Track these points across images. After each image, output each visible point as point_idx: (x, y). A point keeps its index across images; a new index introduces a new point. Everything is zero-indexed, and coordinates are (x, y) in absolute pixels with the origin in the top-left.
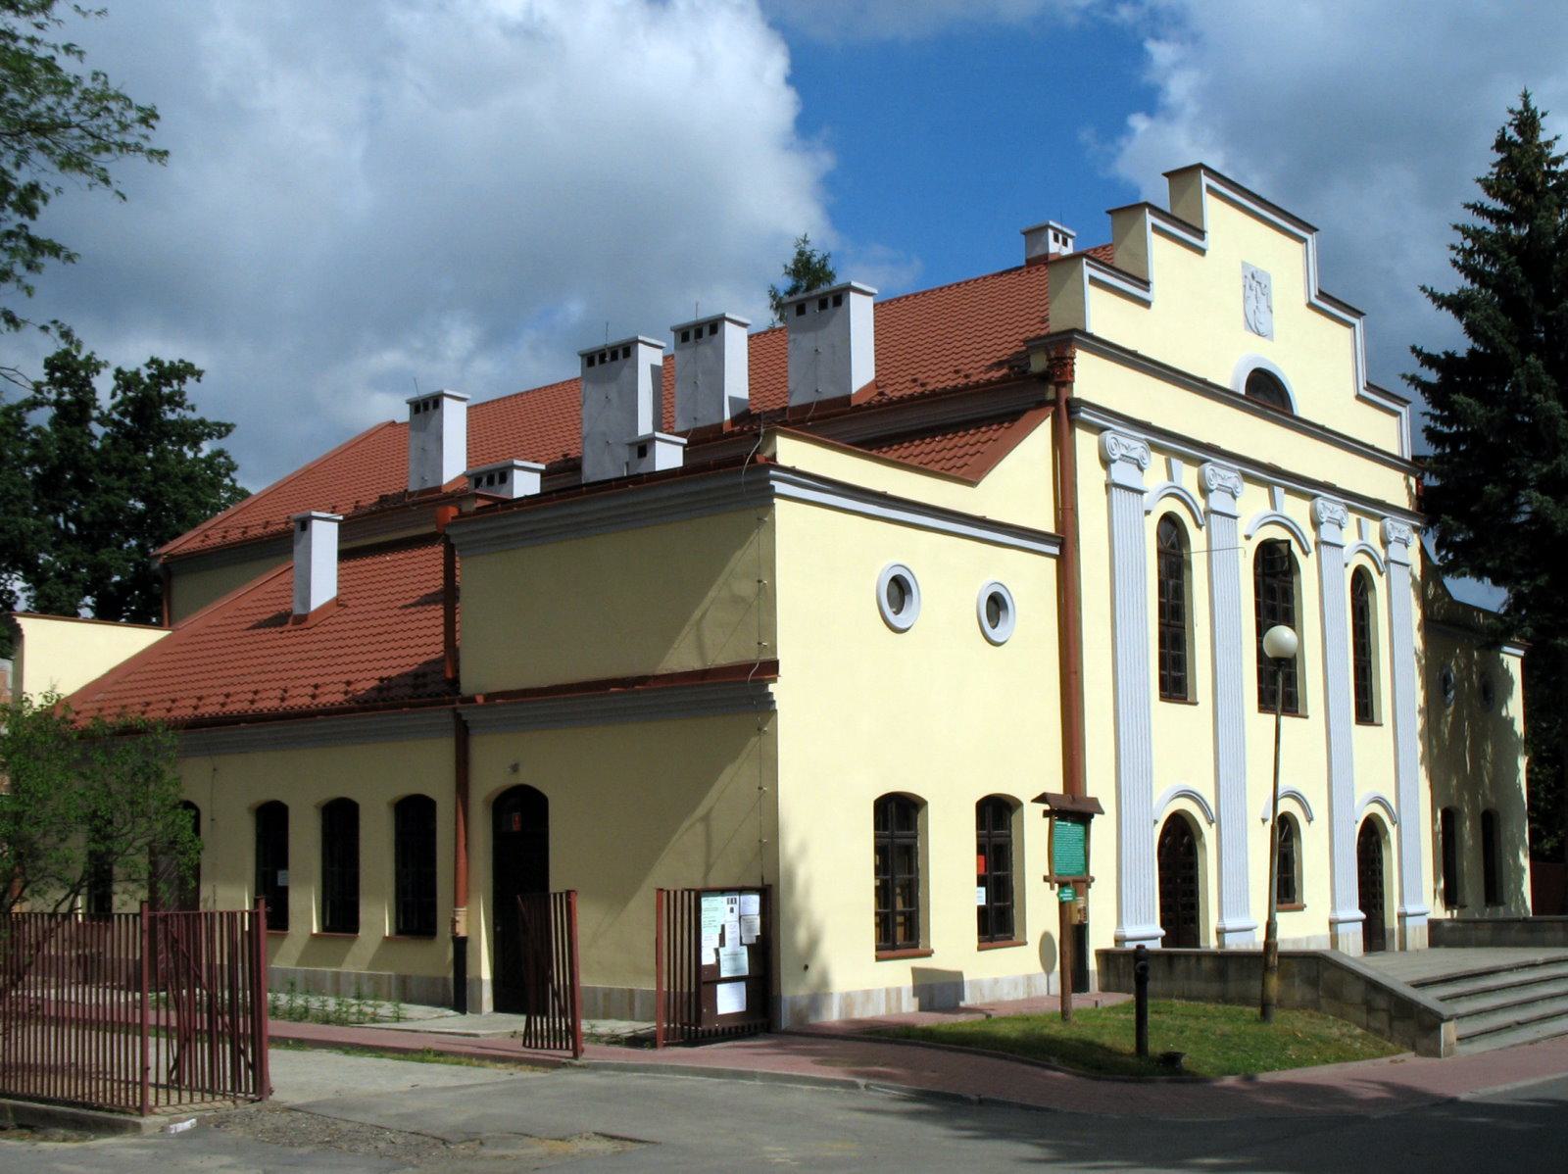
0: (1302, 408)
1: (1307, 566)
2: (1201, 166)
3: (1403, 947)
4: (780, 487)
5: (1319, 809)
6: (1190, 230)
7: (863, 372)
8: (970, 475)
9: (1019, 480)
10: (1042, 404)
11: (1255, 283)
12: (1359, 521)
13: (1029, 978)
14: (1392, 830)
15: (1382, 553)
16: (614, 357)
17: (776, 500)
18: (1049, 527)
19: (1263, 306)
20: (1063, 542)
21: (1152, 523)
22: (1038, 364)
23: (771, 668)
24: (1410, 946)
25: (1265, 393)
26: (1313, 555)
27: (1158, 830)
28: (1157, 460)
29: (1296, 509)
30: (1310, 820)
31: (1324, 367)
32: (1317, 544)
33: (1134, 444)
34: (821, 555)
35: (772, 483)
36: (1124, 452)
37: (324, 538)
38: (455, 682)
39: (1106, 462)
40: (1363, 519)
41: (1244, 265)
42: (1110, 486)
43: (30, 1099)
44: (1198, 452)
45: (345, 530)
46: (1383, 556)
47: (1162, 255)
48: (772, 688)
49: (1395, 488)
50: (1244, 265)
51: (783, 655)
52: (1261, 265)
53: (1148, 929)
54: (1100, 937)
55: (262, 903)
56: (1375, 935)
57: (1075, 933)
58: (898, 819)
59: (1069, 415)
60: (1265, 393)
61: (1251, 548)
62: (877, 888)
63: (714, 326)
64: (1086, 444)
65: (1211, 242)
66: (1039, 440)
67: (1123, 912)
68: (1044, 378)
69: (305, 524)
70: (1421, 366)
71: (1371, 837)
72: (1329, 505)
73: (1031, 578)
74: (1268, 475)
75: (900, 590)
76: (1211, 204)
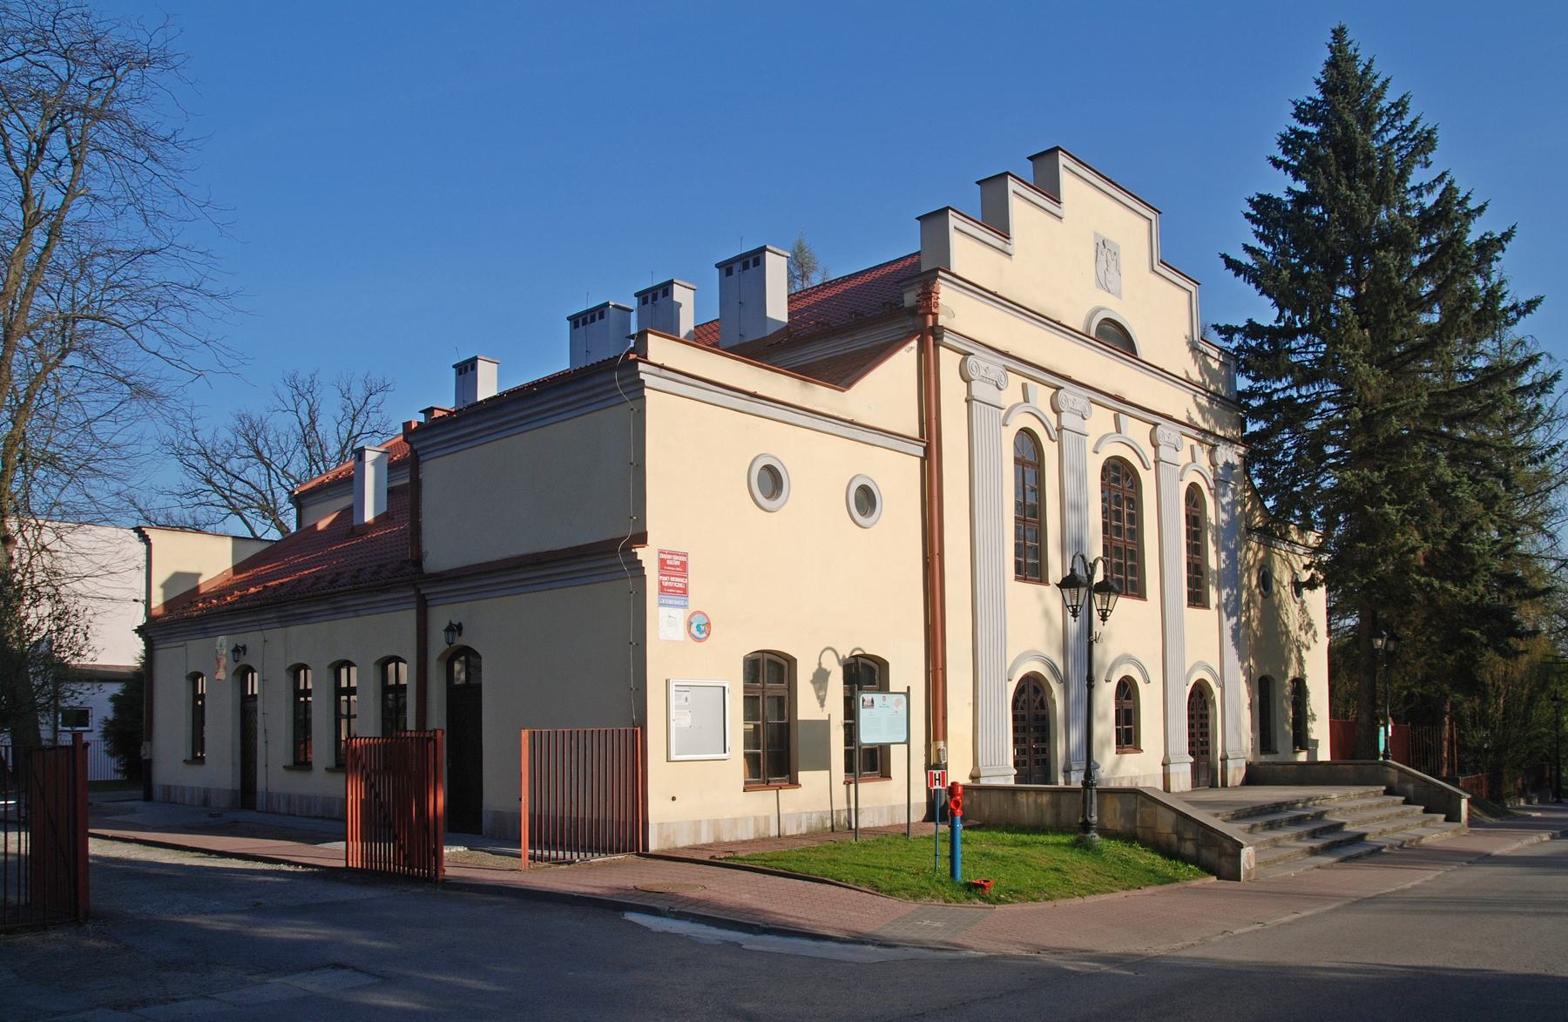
1: (1147, 479)
2: (1057, 149)
3: (1224, 784)
4: (649, 380)
5: (1156, 677)
9: (889, 386)
11: (1104, 248)
12: (1024, 386)
13: (893, 808)
14: (1217, 691)
15: (1052, 418)
16: (593, 320)
17: (647, 392)
18: (913, 429)
19: (1112, 268)
21: (1009, 436)
22: (910, 299)
23: (642, 539)
25: (1115, 338)
27: (1188, 689)
28: (1015, 381)
31: (1165, 318)
33: (994, 366)
34: (699, 436)
35: (642, 376)
38: (418, 562)
40: (1029, 382)
41: (1096, 235)
43: (1035, 790)
44: (1060, 380)
46: (1055, 425)
47: (1022, 209)
48: (641, 553)
49: (1182, 404)
50: (1096, 235)
52: (1110, 236)
53: (1001, 772)
56: (1205, 769)
58: (769, 674)
59: (930, 335)
60: (1115, 338)
62: (150, 738)
64: (948, 362)
66: (905, 359)
67: (981, 750)
68: (913, 311)
70: (1250, 321)
71: (1200, 698)
72: (983, 364)
73: (897, 477)
75: (772, 481)
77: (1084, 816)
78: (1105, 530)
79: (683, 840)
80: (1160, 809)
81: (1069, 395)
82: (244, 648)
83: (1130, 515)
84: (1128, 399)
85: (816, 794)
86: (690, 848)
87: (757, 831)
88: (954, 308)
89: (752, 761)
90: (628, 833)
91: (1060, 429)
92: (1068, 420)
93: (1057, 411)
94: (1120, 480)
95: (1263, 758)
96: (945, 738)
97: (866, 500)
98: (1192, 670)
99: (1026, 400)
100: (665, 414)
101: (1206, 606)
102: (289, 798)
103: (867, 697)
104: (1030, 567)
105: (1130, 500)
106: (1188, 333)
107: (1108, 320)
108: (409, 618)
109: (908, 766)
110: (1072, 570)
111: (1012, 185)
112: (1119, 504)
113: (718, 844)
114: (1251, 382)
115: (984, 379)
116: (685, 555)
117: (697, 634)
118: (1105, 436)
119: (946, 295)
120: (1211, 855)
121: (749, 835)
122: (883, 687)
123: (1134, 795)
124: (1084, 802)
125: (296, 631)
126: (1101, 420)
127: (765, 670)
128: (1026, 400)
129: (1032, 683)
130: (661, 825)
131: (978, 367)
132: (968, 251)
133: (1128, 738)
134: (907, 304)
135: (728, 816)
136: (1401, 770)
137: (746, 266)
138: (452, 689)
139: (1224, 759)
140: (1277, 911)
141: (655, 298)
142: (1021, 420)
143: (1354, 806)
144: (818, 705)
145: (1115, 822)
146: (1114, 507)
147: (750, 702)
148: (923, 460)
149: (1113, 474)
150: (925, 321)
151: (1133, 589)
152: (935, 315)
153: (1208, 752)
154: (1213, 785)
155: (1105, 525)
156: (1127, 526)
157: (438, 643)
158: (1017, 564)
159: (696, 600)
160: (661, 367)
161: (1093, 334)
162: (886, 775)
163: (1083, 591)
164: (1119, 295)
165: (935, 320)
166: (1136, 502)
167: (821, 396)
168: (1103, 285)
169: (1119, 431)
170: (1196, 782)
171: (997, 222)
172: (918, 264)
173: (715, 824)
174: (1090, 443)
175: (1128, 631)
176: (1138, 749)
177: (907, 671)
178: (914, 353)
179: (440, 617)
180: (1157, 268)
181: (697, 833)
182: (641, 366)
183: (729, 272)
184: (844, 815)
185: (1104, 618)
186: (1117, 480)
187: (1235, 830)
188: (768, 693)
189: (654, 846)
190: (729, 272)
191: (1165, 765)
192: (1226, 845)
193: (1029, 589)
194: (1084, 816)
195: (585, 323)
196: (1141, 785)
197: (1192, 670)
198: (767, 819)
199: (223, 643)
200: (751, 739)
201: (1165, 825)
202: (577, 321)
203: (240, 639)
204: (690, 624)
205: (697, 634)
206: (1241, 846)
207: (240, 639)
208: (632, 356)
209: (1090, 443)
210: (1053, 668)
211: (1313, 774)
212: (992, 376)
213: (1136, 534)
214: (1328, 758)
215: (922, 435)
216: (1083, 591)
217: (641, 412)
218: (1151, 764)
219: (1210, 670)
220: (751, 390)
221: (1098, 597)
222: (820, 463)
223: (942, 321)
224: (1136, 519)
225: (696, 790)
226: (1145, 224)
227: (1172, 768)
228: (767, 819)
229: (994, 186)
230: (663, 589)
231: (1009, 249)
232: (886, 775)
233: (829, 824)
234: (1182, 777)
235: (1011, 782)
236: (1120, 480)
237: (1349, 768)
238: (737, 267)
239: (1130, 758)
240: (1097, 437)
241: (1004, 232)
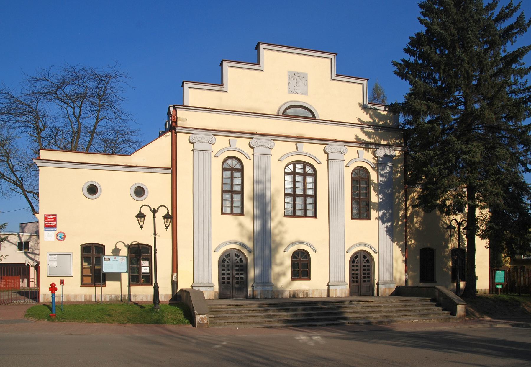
12: (296, 145)
64: (182, 139)
85: (112, 290)
87: (86, 299)
95: (421, 284)
101: (368, 218)
106: (361, 101)
116: (56, 215)
117: (60, 239)
121: (83, 300)
129: (362, 254)
135: (311, 289)
148: (172, 174)
159: (59, 228)
176: (309, 279)
178: (170, 137)
184: (127, 297)
198: (91, 296)
204: (57, 236)
205: (60, 239)
210: (243, 245)
220: (125, 164)
227: (331, 287)
228: (91, 296)
230: (46, 226)
231: (223, 89)
233: (120, 299)
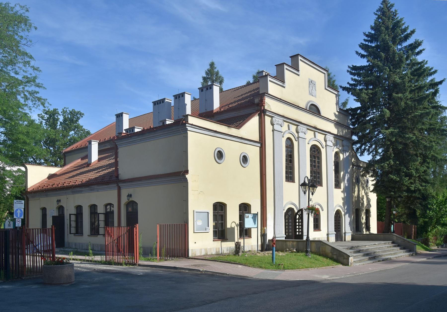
0: (323, 114)
1: (323, 151)
2: (298, 54)
3: (345, 240)
4: (189, 128)
6: (295, 67)
7: (216, 105)
8: (238, 127)
9: (251, 128)
10: (257, 111)
11: (311, 83)
12: (288, 125)
15: (296, 134)
16: (160, 103)
17: (188, 132)
18: (257, 138)
20: (262, 142)
21: (284, 140)
22: (257, 101)
23: (187, 172)
24: (347, 240)
25: (314, 110)
26: (325, 148)
27: (335, 212)
28: (286, 124)
29: (320, 137)
30: (323, 210)
31: (329, 105)
32: (326, 146)
34: (200, 142)
36: (277, 122)
37: (95, 147)
38: (117, 177)
39: (272, 124)
41: (309, 79)
42: (273, 130)
43: (292, 241)
44: (298, 123)
45: (99, 144)
47: (288, 74)
48: (187, 176)
50: (309, 79)
51: (189, 169)
53: (281, 235)
54: (270, 236)
55: (53, 226)
56: (339, 236)
57: (264, 236)
58: (220, 209)
59: (262, 113)
60: (314, 110)
61: (309, 146)
63: (183, 95)
64: (267, 120)
65: (301, 73)
66: (255, 120)
67: (276, 229)
69: (90, 143)
71: (338, 215)
72: (277, 120)
73: (253, 152)
74: (315, 129)
75: (220, 155)
76: (301, 63)
77: (306, 249)
78: (311, 166)
79: (198, 254)
80: (327, 247)
81: (302, 128)
82: (60, 200)
83: (318, 162)
84: (318, 127)
86: (200, 256)
87: (216, 252)
88: (270, 104)
89: (215, 233)
90: (183, 252)
91: (298, 137)
92: (301, 135)
93: (298, 132)
94: (315, 152)
96: (266, 226)
97: (245, 159)
98: (335, 208)
99: (289, 129)
100: (193, 137)
102: (76, 244)
103: (247, 215)
104: (290, 177)
105: (318, 157)
107: (312, 105)
108: (115, 192)
109: (255, 233)
110: (304, 181)
111: (285, 67)
112: (315, 158)
113: (206, 255)
114: (354, 125)
115: (277, 124)
118: (311, 139)
119: (267, 100)
120: (339, 258)
121: (214, 253)
122: (249, 212)
123: (319, 242)
124: (306, 245)
125: (77, 196)
126: (310, 134)
127: (219, 208)
128: (289, 129)
130: (192, 250)
131: (276, 121)
132: (273, 88)
133: (317, 227)
134: (255, 102)
136: (397, 236)
137: (207, 89)
138: (128, 213)
139: (345, 233)
140: (358, 270)
141: (179, 97)
142: (287, 135)
143: (383, 248)
144: (232, 218)
145: (314, 249)
146: (313, 159)
147: (215, 216)
148: (260, 147)
149: (313, 150)
150: (261, 108)
151: (319, 183)
152: (264, 106)
153: (340, 231)
154: (342, 240)
155: (311, 165)
156: (317, 165)
157: (124, 200)
158: (286, 177)
160: (192, 125)
161: (308, 109)
162: (250, 237)
163: (307, 187)
164: (315, 96)
165: (264, 108)
166: (320, 158)
167: (233, 131)
168: (311, 94)
169: (315, 137)
170: (337, 239)
171: (280, 78)
172: (259, 91)
173: (206, 250)
174: (307, 141)
175: (319, 197)
177: (256, 208)
179: (125, 193)
180: (327, 88)
181: (201, 252)
182: (187, 125)
183: (202, 91)
185: (312, 194)
186: (314, 151)
187: (348, 252)
188: (219, 214)
189: (190, 255)
190: (202, 91)
191: (328, 235)
192: (345, 256)
193: (290, 184)
194: (306, 249)
195: (158, 104)
196: (321, 240)
197: (336, 207)
198: (219, 248)
199: (55, 199)
200: (215, 227)
201: (328, 250)
202: (155, 103)
203: (59, 198)
206: (349, 256)
207: (59, 198)
208: (184, 122)
209: (307, 141)
211: (371, 238)
212: (280, 123)
213: (320, 167)
214: (375, 232)
215: (260, 140)
216: (307, 187)
217: (186, 137)
218: (323, 234)
219: (340, 206)
220: (215, 130)
221: (311, 188)
222: (233, 150)
223: (266, 107)
224: (320, 163)
225: (201, 242)
226: (323, 75)
228: (219, 248)
229: (280, 67)
231: (284, 85)
232: (250, 237)
234: (332, 239)
235: (284, 239)
236: (315, 152)
237: (382, 236)
238: (205, 89)
239: (317, 233)
240: (309, 139)
241: (283, 82)
